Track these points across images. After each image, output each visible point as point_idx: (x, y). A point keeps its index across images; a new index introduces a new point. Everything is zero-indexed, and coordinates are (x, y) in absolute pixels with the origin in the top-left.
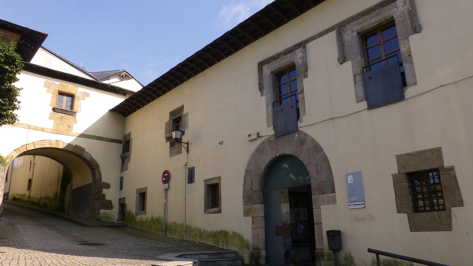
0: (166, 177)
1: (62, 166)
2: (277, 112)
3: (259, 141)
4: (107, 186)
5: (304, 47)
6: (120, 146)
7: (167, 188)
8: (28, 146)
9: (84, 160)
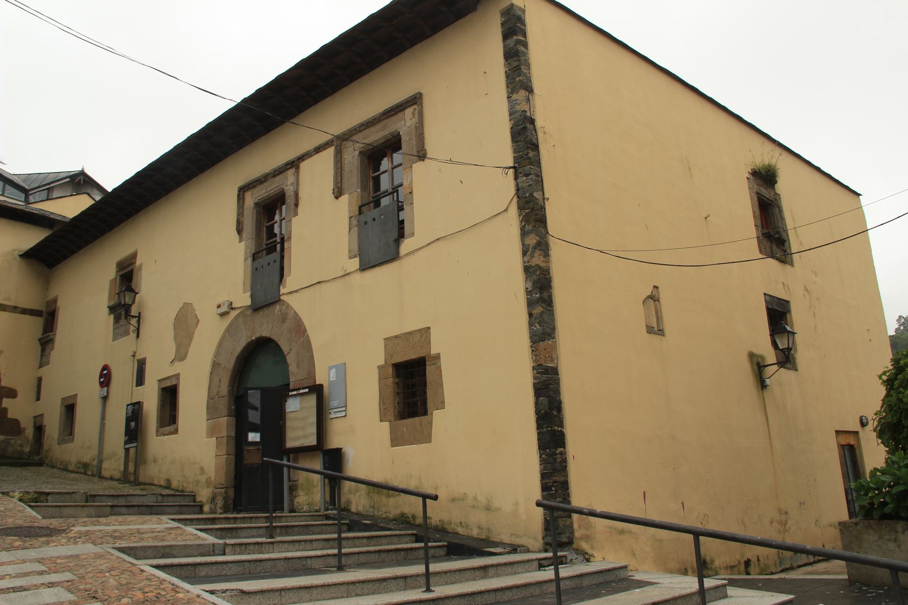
0: (106, 378)
3: (234, 314)
5: (298, 168)
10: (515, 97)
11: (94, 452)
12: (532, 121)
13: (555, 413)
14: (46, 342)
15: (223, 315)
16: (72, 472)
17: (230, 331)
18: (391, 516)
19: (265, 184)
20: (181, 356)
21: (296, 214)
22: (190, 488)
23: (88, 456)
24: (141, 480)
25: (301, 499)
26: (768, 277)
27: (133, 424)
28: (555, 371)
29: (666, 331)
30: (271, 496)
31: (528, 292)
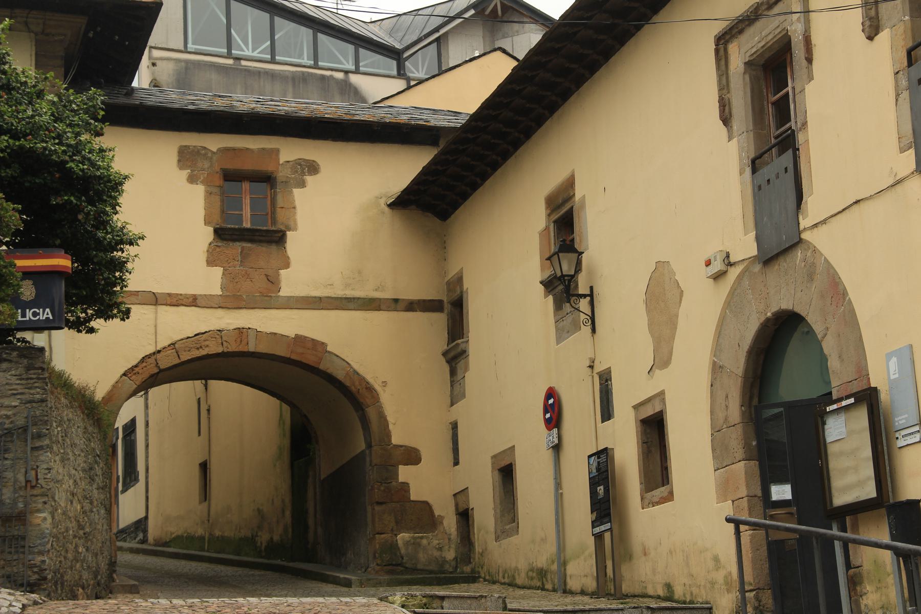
2: (760, 187)
4: (412, 457)
6: (439, 320)
7: (556, 441)
8: (159, 356)
9: (331, 379)
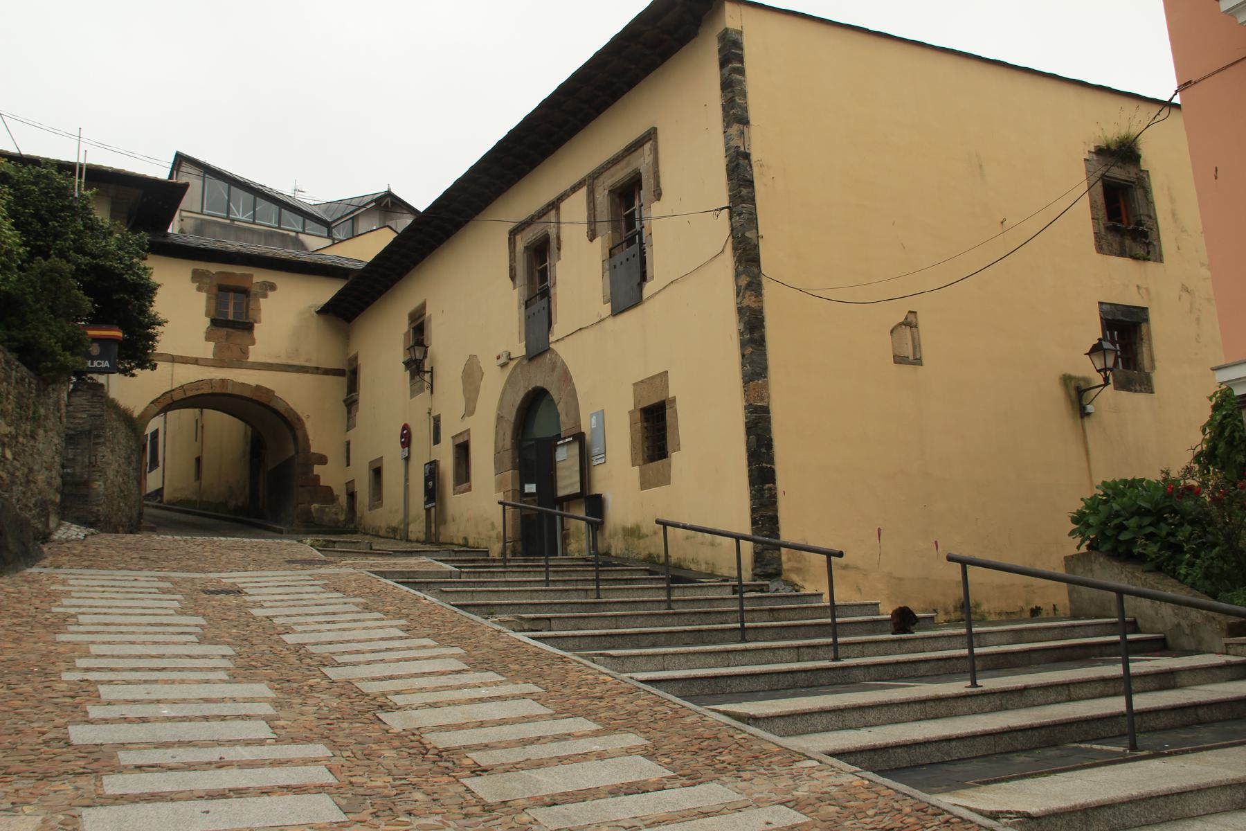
0: (406, 438)
1: (249, 428)
3: (512, 364)
4: (323, 460)
5: (558, 209)
10: (730, 131)
11: (401, 516)
12: (747, 156)
13: (764, 450)
14: (351, 403)
15: (503, 366)
16: (383, 537)
17: (510, 382)
18: (641, 557)
19: (533, 227)
20: (470, 411)
21: (559, 259)
22: (484, 544)
23: (396, 520)
24: (442, 539)
25: (573, 546)
26: (1122, 280)
27: (431, 483)
28: (766, 410)
29: (924, 360)
30: (1105, 747)
31: (741, 334)
